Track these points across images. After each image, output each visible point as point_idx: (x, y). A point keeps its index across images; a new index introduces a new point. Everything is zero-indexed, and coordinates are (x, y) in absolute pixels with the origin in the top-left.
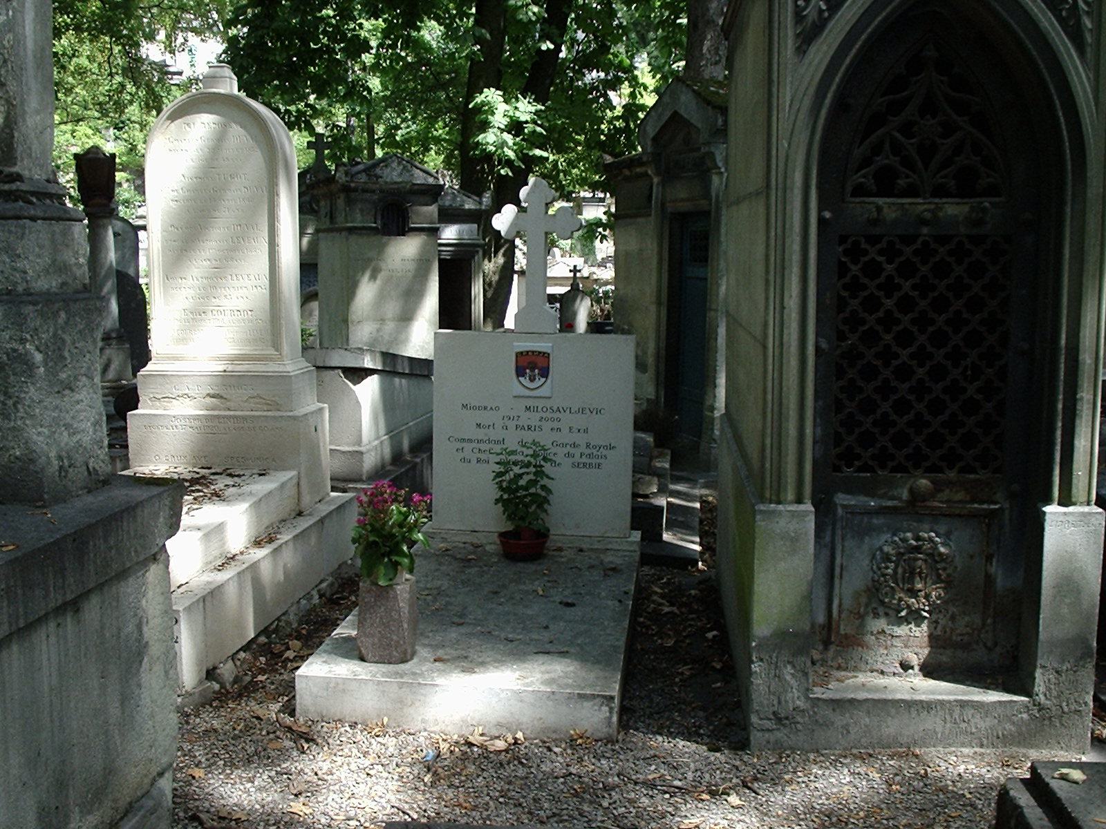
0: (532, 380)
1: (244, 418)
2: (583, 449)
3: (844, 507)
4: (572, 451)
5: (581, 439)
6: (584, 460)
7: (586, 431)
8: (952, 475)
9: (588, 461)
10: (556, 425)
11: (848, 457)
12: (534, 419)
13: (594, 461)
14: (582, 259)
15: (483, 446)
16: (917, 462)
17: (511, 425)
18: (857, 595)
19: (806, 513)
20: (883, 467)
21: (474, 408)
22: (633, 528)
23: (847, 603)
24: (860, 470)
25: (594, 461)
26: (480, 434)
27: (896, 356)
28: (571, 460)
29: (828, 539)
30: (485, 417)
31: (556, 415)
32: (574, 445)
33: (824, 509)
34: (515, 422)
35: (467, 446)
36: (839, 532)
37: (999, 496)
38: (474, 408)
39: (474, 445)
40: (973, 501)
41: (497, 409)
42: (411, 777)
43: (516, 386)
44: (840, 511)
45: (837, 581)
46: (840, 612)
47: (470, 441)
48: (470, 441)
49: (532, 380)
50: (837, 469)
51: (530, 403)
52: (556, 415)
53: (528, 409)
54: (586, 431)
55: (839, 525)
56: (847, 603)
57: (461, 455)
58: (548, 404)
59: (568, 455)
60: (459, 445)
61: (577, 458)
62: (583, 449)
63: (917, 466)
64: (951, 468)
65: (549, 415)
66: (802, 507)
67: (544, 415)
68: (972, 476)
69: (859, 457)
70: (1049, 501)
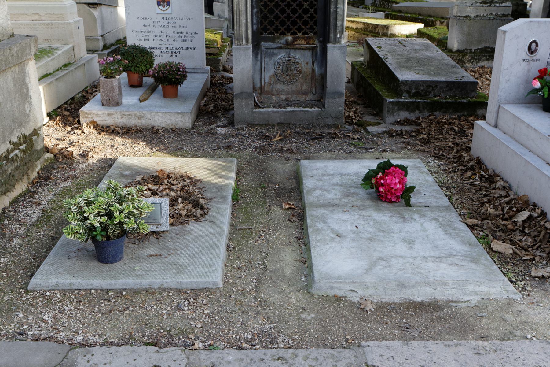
0: (164, 7)
1: (49, 24)
2: (185, 34)
3: (264, 47)
4: (181, 35)
5: (184, 30)
6: (186, 38)
7: (186, 27)
8: (300, 35)
9: (187, 39)
10: (174, 25)
11: (265, 29)
12: (165, 23)
13: (189, 39)
14: (417, 112)
15: (146, 34)
16: (288, 30)
17: (157, 25)
18: (270, 77)
19: (249, 48)
20: (277, 33)
21: (142, 19)
22: (207, 65)
23: (267, 80)
24: (269, 34)
25: (189, 39)
26: (145, 29)
27: (292, 5)
28: (181, 39)
29: (259, 58)
30: (146, 22)
31: (174, 21)
32: (182, 33)
33: (256, 47)
34: (158, 24)
35: (140, 34)
36: (263, 56)
37: (316, 42)
38: (142, 19)
39: (142, 34)
40: (307, 44)
41: (151, 19)
42: (294, 307)
43: (158, 10)
44: (263, 48)
45: (263, 73)
46: (265, 83)
47: (141, 32)
48: (141, 32)
49: (164, 7)
50: (262, 34)
51: (163, 16)
52: (174, 21)
53: (163, 18)
54: (186, 27)
55: (263, 53)
56: (267, 80)
57: (137, 37)
58: (171, 16)
59: (180, 37)
60: (137, 34)
61: (183, 38)
62: (185, 34)
63: (288, 32)
64: (300, 32)
65: (171, 21)
66: (248, 46)
67: (169, 21)
68: (307, 35)
69: (269, 29)
70: (329, 42)
